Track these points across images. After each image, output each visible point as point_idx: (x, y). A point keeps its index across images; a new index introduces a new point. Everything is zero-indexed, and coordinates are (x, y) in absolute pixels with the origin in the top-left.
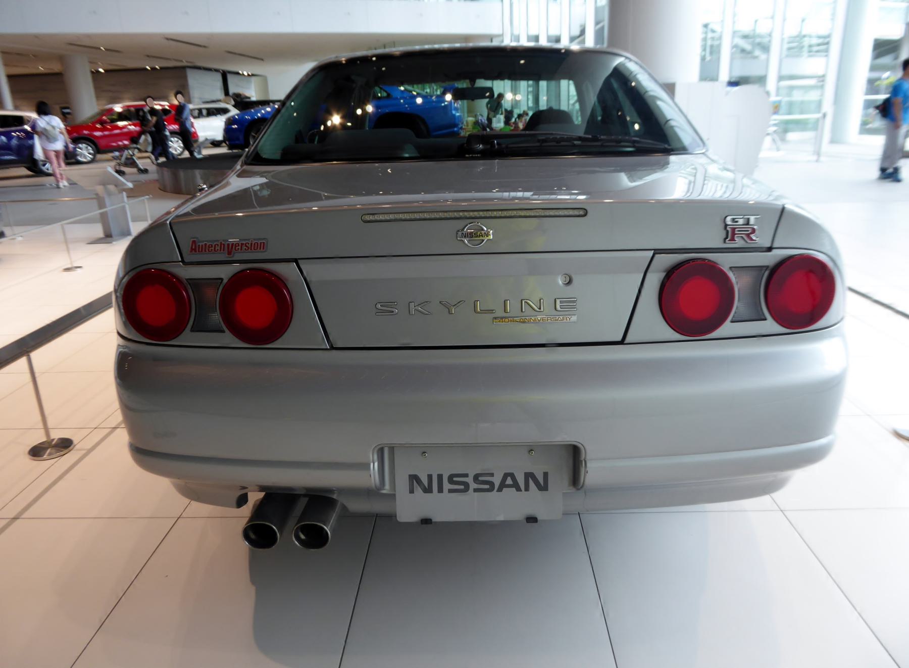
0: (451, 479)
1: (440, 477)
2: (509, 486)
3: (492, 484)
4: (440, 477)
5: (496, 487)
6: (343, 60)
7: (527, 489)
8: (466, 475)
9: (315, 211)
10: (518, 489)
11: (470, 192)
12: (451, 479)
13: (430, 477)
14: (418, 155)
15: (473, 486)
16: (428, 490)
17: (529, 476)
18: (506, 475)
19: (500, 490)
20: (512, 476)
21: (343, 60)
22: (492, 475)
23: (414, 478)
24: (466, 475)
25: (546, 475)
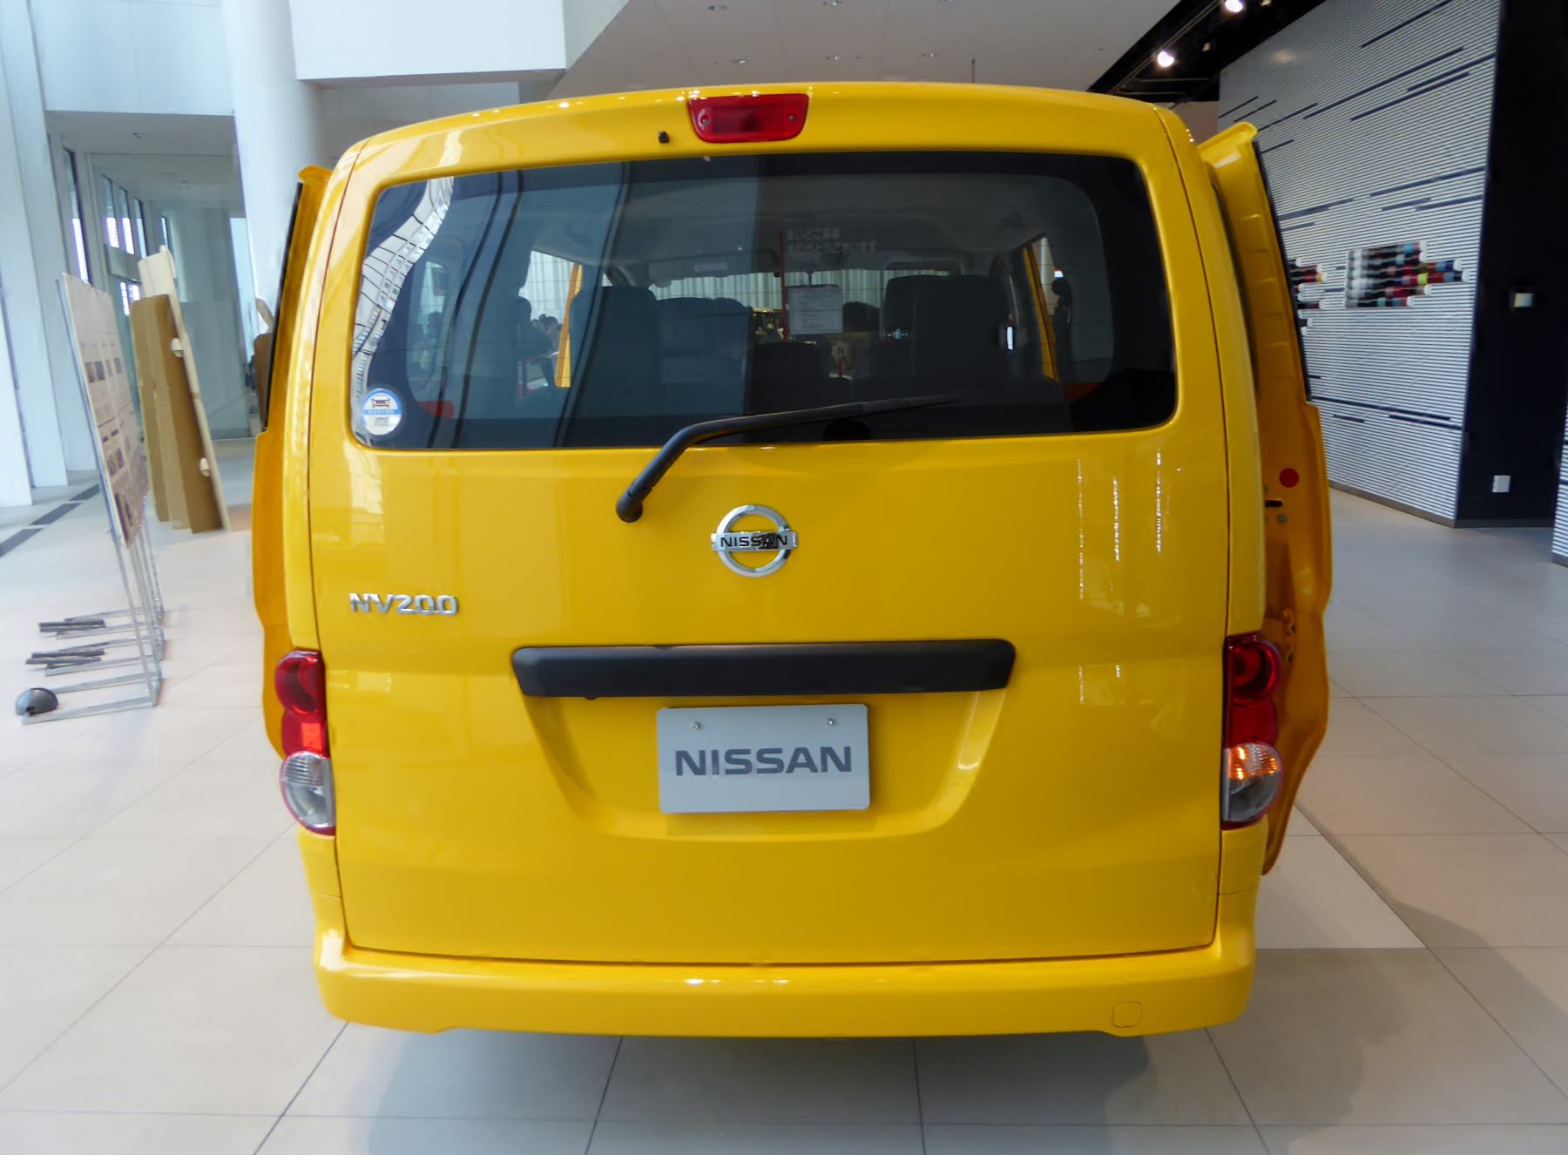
0: (729, 759)
1: (715, 754)
2: (802, 765)
3: (780, 762)
4: (715, 754)
5: (786, 766)
6: (524, 292)
7: (825, 769)
8: (747, 752)
9: (998, 338)
10: (814, 770)
11: (761, 97)
12: (729, 754)
13: (702, 754)
14: (494, 197)
15: (752, 758)
16: (699, 771)
17: (827, 752)
18: (798, 751)
19: (790, 770)
20: (805, 751)
21: (524, 292)
22: (779, 751)
23: (682, 756)
24: (747, 752)
25: (847, 750)
